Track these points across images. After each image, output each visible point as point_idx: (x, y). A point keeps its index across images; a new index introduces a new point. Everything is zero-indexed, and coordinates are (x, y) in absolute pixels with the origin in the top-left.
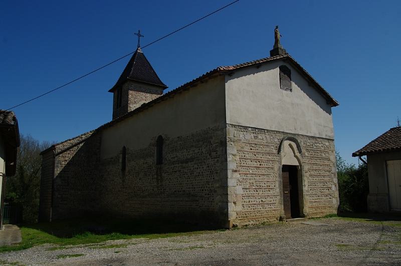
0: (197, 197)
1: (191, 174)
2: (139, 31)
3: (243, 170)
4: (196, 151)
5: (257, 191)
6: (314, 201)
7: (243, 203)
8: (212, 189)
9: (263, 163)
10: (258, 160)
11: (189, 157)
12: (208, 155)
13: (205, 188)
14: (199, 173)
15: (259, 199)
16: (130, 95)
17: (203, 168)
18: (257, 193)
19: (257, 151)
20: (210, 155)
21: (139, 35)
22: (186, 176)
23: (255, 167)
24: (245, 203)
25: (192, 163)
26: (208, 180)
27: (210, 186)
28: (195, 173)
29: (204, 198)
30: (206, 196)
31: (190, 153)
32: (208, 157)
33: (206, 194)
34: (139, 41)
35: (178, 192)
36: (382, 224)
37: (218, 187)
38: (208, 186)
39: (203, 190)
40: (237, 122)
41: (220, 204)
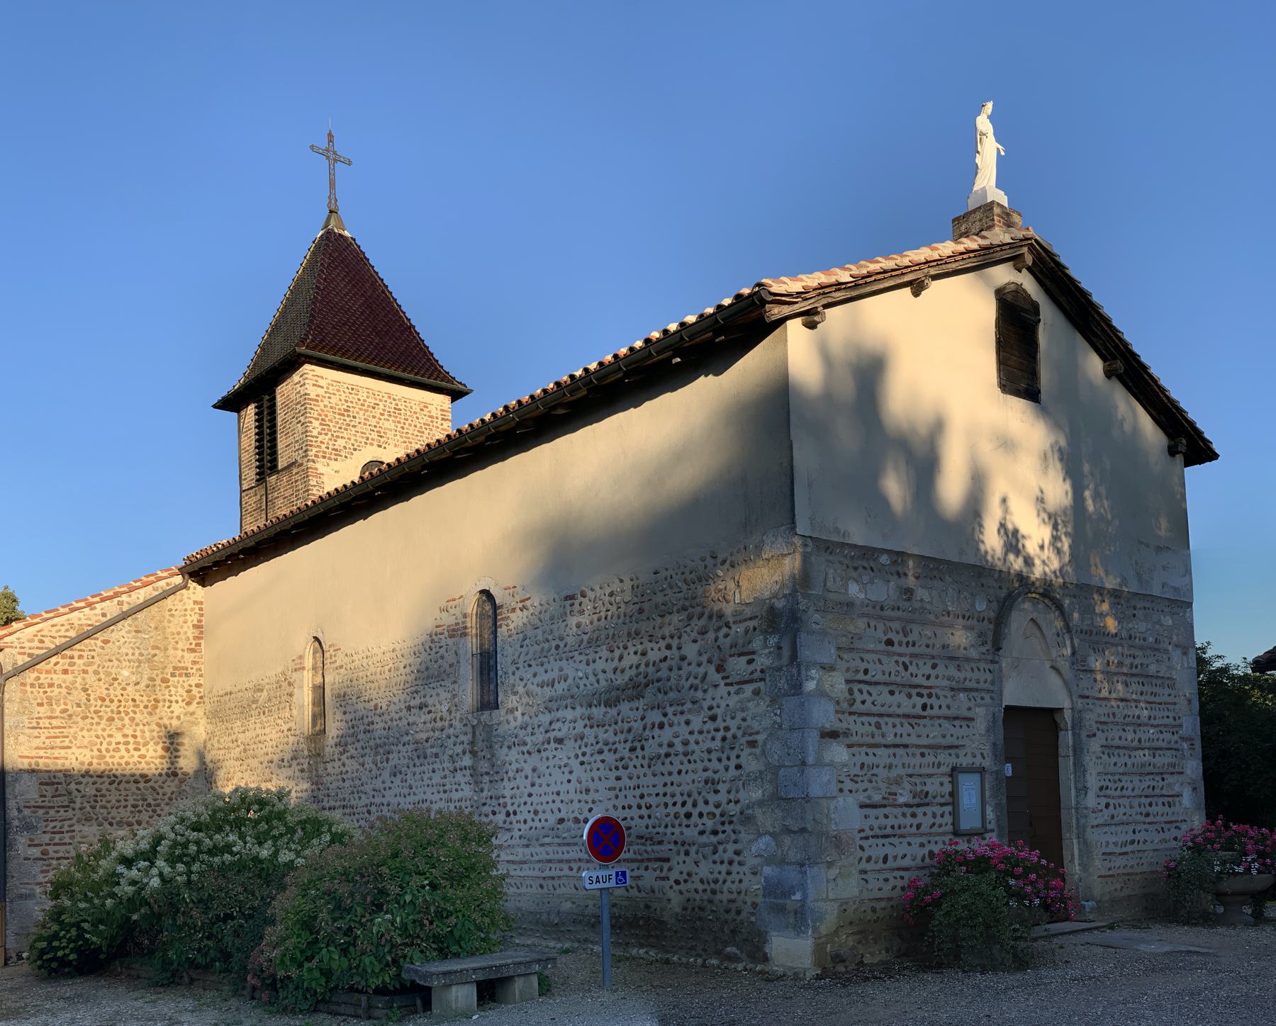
0: (660, 843)
1: (633, 750)
2: (330, 135)
4: (654, 656)
5: (914, 815)
6: (1118, 850)
7: (864, 865)
8: (733, 809)
10: (916, 686)
12: (712, 669)
14: (671, 745)
15: (922, 845)
16: (316, 423)
17: (687, 723)
19: (911, 650)
20: (720, 669)
21: (332, 156)
23: (906, 716)
25: (641, 703)
26: (709, 774)
27: (722, 797)
29: (693, 850)
30: (704, 839)
31: (626, 663)
32: (714, 676)
33: (702, 833)
34: (332, 185)
35: (571, 824)
36: (631, 844)
37: (760, 803)
38: (712, 798)
39: (688, 815)
41: (768, 870)
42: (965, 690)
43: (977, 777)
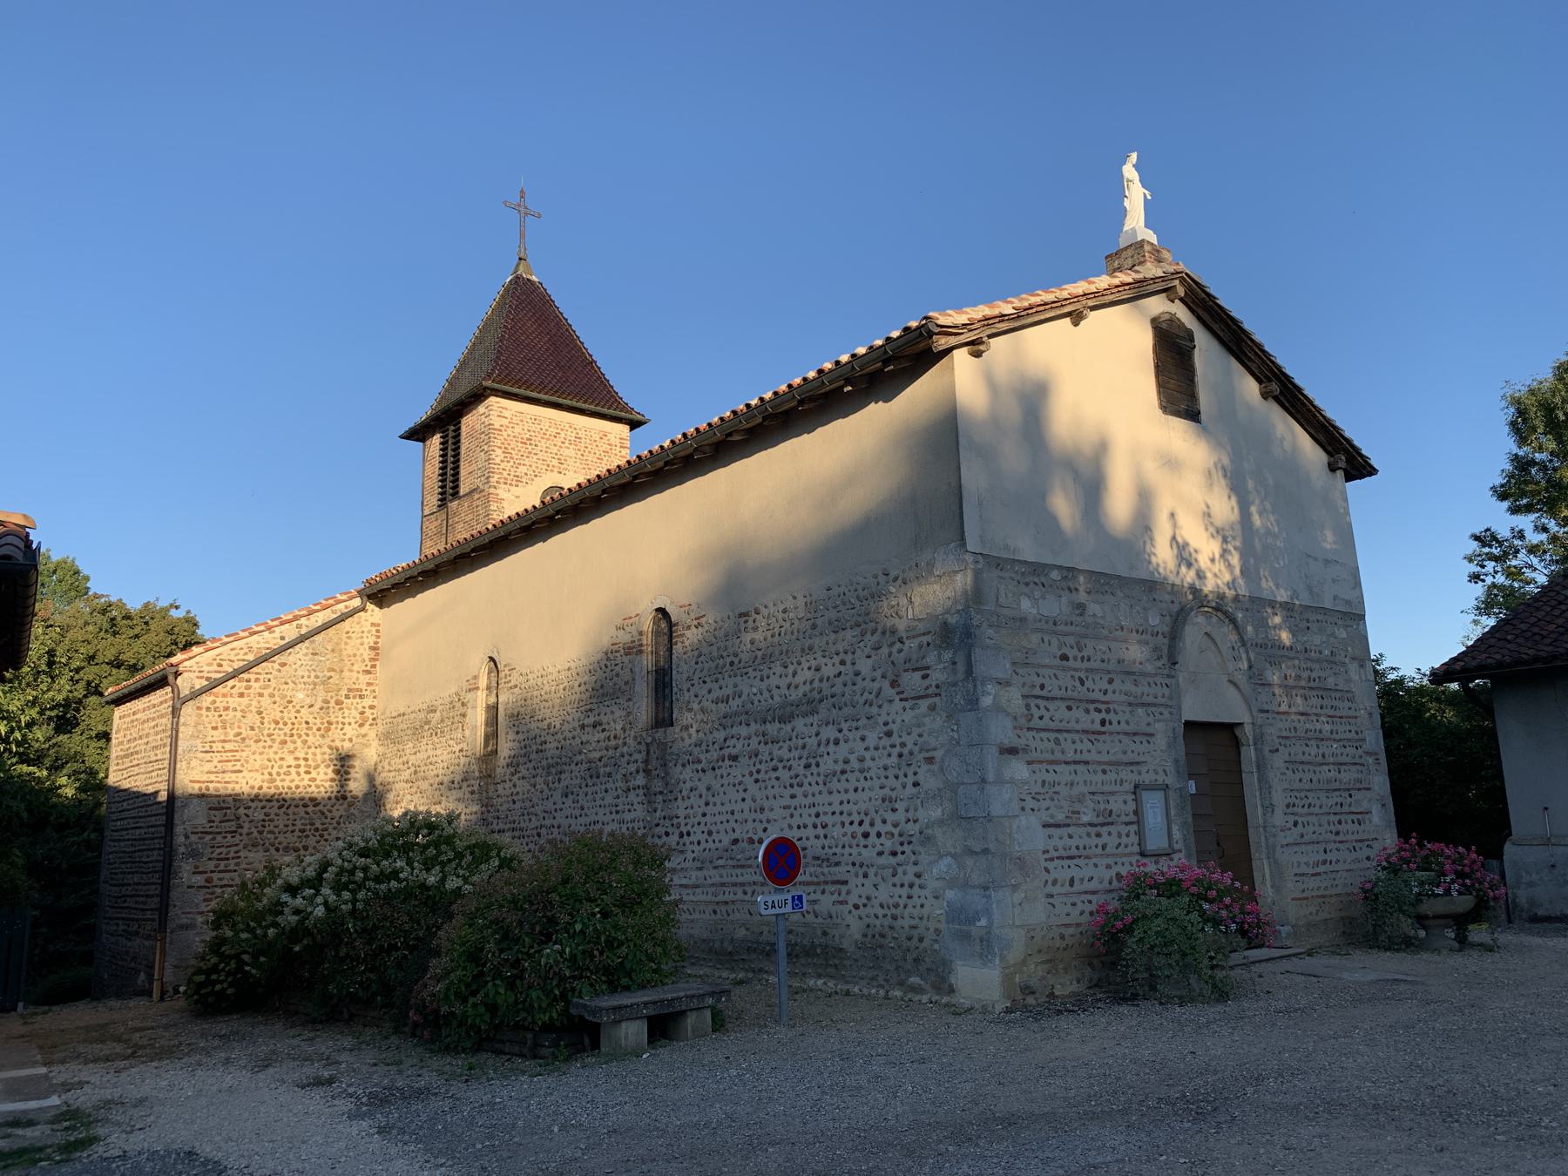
0: (837, 864)
1: (807, 766)
3: (1040, 744)
4: (828, 671)
5: (1098, 835)
7: (1050, 889)
8: (912, 828)
9: (1111, 716)
10: (1093, 702)
11: (795, 695)
12: (886, 684)
13: (879, 827)
15: (1108, 867)
16: (499, 452)
17: (863, 739)
18: (1100, 841)
19: (1086, 665)
20: (894, 684)
21: (522, 210)
22: (784, 775)
23: (1085, 732)
24: (1056, 890)
25: (815, 719)
28: (827, 765)
29: (871, 872)
32: (889, 692)
33: (880, 854)
34: (522, 235)
35: (745, 844)
38: (890, 817)
39: (866, 835)
40: (1007, 547)
41: (950, 894)
42: (1143, 705)
43: (1161, 794)
